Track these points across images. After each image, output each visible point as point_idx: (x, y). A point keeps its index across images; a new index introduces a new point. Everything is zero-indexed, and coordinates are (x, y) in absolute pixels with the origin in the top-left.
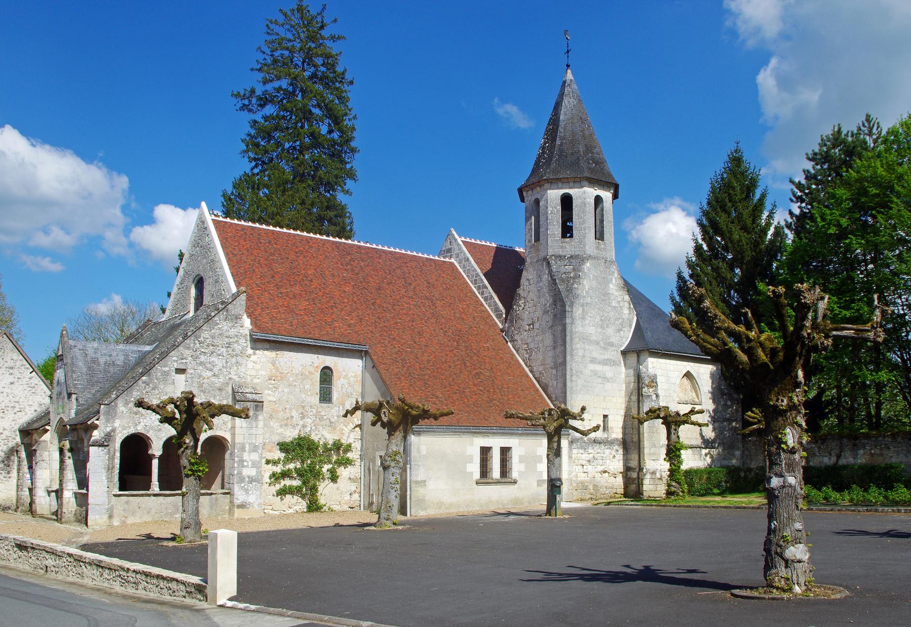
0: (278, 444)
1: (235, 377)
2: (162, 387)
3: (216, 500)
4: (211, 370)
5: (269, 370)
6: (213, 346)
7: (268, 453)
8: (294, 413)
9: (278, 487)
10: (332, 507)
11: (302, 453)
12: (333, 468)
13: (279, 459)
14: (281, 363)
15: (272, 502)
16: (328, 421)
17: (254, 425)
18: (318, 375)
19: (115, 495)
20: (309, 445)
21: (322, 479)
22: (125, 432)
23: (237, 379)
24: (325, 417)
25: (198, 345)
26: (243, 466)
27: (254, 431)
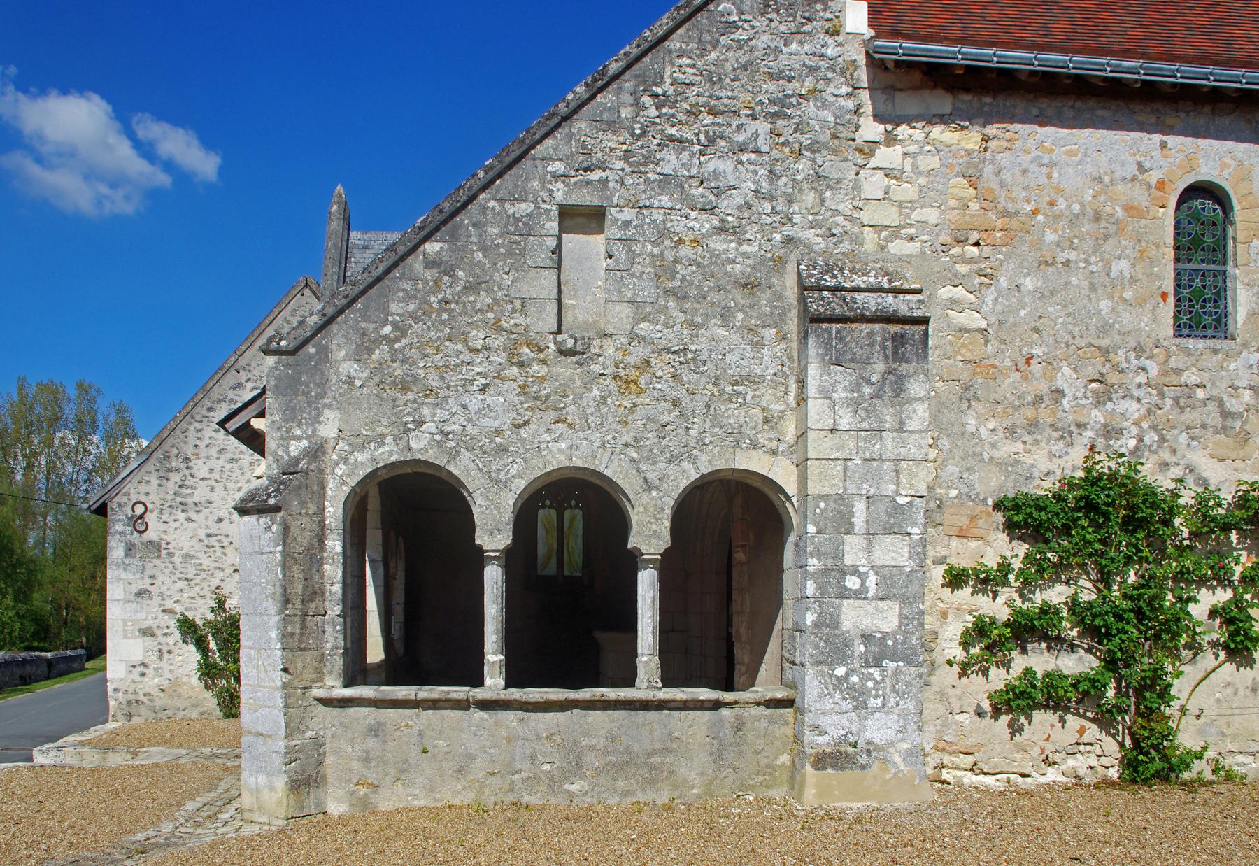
0: (997, 506)
1: (809, 235)
2: (507, 279)
3: (739, 726)
4: (711, 209)
5: (952, 203)
6: (712, 112)
7: (955, 543)
8: (1065, 377)
9: (998, 678)
10: (1229, 761)
11: (1104, 542)
12: (1237, 602)
13: (1004, 567)
14: (1006, 176)
15: (972, 740)
16: (1212, 407)
17: (889, 421)
18: (1167, 217)
19: (327, 702)
20: (1132, 508)
21: (1188, 646)
22: (362, 457)
23: (820, 244)
24: (1200, 394)
25: (653, 112)
26: (844, 594)
27: (889, 445)
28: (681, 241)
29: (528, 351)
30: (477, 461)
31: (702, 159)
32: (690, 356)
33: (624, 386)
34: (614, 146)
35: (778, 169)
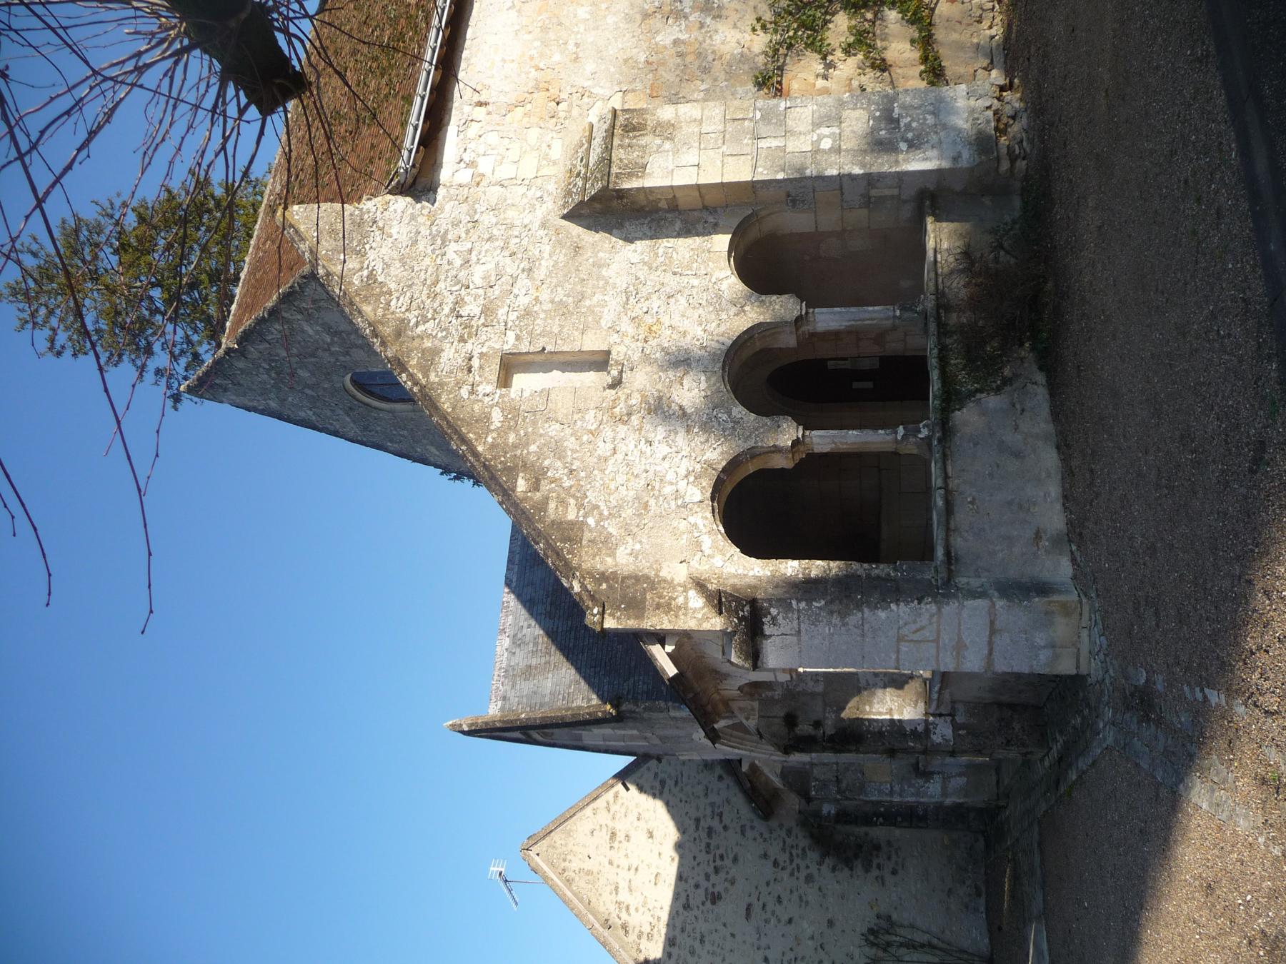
1: (541, 212)
4: (515, 279)
6: (436, 283)
22: (707, 542)
25: (430, 324)
28: (537, 299)
29: (619, 407)
30: (715, 446)
31: (471, 287)
32: (631, 288)
33: (654, 335)
34: (453, 351)
35: (486, 236)
